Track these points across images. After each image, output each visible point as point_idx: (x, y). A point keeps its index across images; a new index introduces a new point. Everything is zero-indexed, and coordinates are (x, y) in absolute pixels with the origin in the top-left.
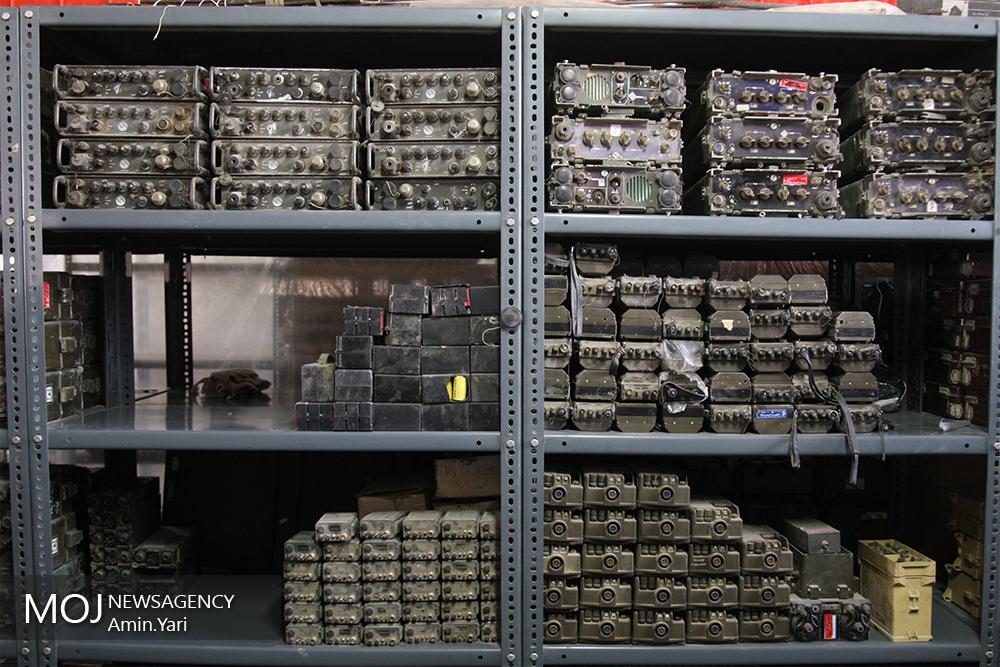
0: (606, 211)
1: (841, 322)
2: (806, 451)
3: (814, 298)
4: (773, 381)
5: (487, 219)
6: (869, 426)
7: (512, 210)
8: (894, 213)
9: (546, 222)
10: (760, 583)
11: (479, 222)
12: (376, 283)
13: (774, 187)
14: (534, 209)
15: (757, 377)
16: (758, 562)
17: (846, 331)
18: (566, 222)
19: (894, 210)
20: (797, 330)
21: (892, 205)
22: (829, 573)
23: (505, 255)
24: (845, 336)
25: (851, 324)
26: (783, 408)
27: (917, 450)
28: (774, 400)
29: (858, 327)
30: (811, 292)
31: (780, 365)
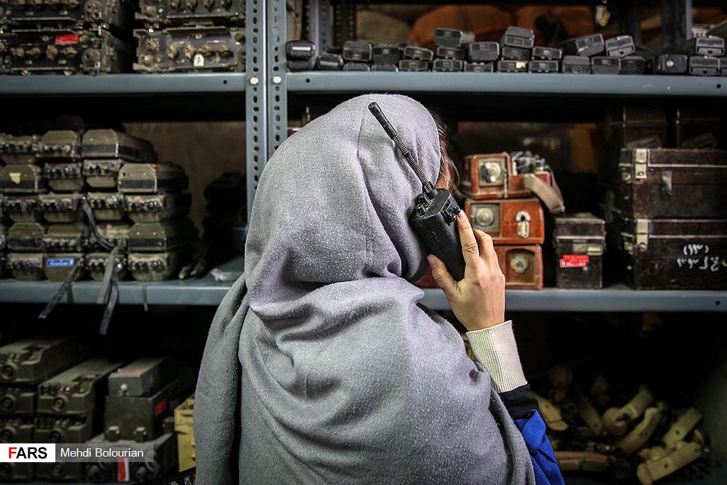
0: (186, 71)
1: (124, 174)
2: (124, 300)
3: (105, 151)
4: (63, 231)
5: (234, 79)
6: (160, 275)
7: (256, 70)
8: (162, 68)
9: (287, 80)
10: (52, 424)
11: (225, 82)
12: (642, 153)
13: (44, 47)
14: (276, 69)
15: (51, 227)
16: (50, 404)
17: (128, 183)
18: (308, 81)
19: (162, 65)
20: (93, 182)
21: (159, 60)
22: (129, 416)
23: (250, 123)
24: (128, 187)
25: (133, 176)
26: (71, 257)
27: (179, 301)
28: (63, 249)
29: (140, 179)
30: (102, 146)
31: (67, 216)
